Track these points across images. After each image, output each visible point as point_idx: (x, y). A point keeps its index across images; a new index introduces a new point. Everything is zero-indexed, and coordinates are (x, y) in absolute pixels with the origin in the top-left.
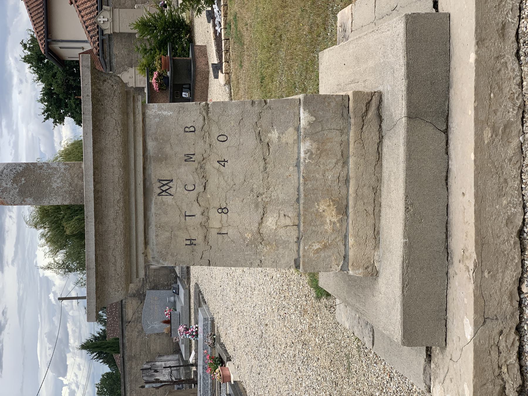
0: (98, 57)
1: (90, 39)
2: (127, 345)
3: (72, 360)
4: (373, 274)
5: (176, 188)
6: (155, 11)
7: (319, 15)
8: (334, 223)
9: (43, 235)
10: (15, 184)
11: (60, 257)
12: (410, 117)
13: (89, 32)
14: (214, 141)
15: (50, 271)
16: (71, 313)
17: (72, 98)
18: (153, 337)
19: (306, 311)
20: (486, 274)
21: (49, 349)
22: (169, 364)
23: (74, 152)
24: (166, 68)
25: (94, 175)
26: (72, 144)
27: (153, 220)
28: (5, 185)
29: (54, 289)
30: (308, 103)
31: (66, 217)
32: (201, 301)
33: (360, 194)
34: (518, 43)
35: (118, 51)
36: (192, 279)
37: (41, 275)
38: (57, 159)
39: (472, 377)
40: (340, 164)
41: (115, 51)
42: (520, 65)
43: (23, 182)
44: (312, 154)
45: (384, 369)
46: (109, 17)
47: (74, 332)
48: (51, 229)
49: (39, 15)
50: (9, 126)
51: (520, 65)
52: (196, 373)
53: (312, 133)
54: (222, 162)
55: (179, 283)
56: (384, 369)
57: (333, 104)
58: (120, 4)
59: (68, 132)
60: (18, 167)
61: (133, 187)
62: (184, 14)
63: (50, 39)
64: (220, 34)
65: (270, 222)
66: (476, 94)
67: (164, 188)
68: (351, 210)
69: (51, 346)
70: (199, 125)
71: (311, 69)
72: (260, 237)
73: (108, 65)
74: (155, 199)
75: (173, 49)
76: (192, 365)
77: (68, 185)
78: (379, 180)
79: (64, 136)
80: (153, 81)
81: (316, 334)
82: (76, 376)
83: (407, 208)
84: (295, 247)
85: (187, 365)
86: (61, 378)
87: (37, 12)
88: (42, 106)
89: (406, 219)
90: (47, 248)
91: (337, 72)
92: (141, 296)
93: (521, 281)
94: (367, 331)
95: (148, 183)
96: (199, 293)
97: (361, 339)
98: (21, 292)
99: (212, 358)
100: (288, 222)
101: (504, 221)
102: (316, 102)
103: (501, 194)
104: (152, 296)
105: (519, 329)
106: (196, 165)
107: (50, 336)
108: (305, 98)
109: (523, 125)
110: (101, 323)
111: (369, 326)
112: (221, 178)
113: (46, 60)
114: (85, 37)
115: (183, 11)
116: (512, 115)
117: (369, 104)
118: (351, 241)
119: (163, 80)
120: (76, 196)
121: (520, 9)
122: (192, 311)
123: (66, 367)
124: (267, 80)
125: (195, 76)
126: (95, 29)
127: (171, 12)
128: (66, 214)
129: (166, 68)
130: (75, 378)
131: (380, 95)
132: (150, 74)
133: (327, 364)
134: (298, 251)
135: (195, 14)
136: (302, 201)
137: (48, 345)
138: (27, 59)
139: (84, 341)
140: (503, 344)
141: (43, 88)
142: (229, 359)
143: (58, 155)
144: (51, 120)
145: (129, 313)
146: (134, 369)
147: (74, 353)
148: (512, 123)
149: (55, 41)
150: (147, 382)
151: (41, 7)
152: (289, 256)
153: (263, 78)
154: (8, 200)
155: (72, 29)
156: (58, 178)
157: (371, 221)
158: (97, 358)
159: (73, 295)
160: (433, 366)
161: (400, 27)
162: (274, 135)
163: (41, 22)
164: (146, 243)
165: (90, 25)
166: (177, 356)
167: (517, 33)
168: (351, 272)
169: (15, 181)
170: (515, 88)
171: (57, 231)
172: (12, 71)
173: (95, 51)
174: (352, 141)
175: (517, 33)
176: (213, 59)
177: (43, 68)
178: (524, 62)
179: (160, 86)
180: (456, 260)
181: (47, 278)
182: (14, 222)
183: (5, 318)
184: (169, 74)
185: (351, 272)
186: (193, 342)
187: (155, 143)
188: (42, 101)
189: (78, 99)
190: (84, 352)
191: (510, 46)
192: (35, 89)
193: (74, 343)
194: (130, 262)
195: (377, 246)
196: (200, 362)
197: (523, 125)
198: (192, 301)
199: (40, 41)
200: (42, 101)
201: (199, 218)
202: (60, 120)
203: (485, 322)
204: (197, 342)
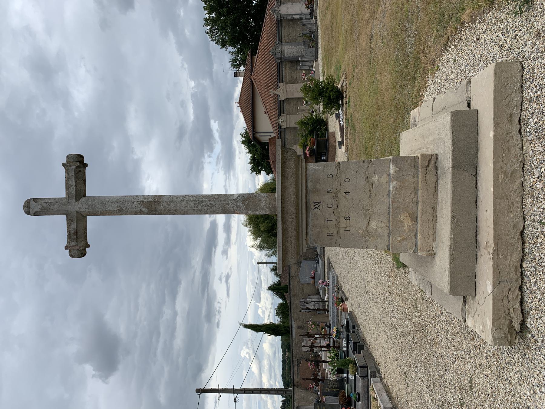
2: (292, 288)
4: (432, 255)
5: (322, 206)
6: (308, 115)
7: (399, 113)
8: (410, 226)
9: (250, 230)
11: (258, 242)
12: (454, 167)
14: (343, 182)
16: (263, 270)
18: (305, 285)
19: (391, 275)
20: (500, 256)
22: (314, 300)
23: (269, 188)
24: (313, 144)
27: (310, 223)
29: (255, 257)
30: (394, 161)
32: (331, 267)
33: (424, 210)
34: (520, 125)
35: (289, 136)
36: (326, 255)
39: (491, 314)
40: (413, 194)
42: (522, 137)
44: (397, 188)
45: (437, 308)
47: (264, 280)
48: (254, 227)
50: (234, 175)
51: (522, 137)
52: (328, 306)
53: (397, 177)
54: (347, 193)
55: (319, 257)
56: (437, 308)
57: (409, 161)
59: (263, 178)
61: (300, 205)
62: (323, 116)
64: (343, 125)
65: (373, 225)
66: (494, 154)
67: (316, 206)
68: (419, 219)
70: (335, 173)
71: (395, 143)
72: (367, 233)
74: (311, 211)
75: (317, 134)
76: (326, 301)
78: (436, 203)
79: (260, 180)
80: (307, 151)
81: (397, 288)
83: (452, 218)
84: (387, 239)
85: (324, 301)
86: (258, 304)
88: (250, 166)
89: (452, 224)
90: (252, 237)
91: (410, 143)
92: (299, 264)
93: (522, 261)
94: (428, 287)
95: (308, 204)
96: (330, 263)
97: (424, 291)
99: (337, 298)
100: (383, 225)
101: (512, 226)
102: (399, 160)
103: (509, 211)
104: (304, 263)
105: (521, 288)
106: (333, 194)
108: (393, 158)
109: (523, 172)
111: (429, 284)
112: (346, 201)
114: (271, 130)
115: (323, 114)
116: (517, 166)
117: (430, 160)
118: (419, 236)
119: (312, 151)
121: (521, 106)
122: (326, 273)
123: (260, 298)
124: (369, 149)
125: (329, 148)
127: (316, 115)
129: (313, 144)
131: (437, 156)
132: (305, 148)
133: (403, 304)
134: (389, 241)
135: (329, 115)
136: (391, 214)
137: (252, 286)
138: (243, 142)
140: (511, 296)
142: (347, 299)
144: (255, 172)
145: (293, 272)
146: (295, 302)
148: (517, 170)
150: (302, 309)
152: (384, 244)
153: (366, 148)
154: (240, 212)
155: (266, 127)
157: (431, 225)
159: (264, 261)
160: (467, 307)
161: (448, 118)
162: (376, 178)
164: (307, 235)
166: (318, 296)
167: (520, 119)
168: (419, 253)
169: (243, 202)
170: (518, 151)
173: (277, 137)
174: (420, 181)
175: (520, 119)
176: (339, 139)
178: (524, 136)
179: (310, 154)
180: (482, 248)
184: (315, 147)
185: (419, 253)
186: (327, 289)
187: (312, 183)
188: (250, 163)
190: (270, 291)
191: (515, 127)
192: (246, 157)
193: (265, 286)
194: (299, 244)
195: (434, 239)
196: (331, 300)
197: (523, 172)
198: (326, 267)
200: (250, 163)
201: (334, 222)
202: (259, 172)
203: (500, 283)
204: (329, 289)
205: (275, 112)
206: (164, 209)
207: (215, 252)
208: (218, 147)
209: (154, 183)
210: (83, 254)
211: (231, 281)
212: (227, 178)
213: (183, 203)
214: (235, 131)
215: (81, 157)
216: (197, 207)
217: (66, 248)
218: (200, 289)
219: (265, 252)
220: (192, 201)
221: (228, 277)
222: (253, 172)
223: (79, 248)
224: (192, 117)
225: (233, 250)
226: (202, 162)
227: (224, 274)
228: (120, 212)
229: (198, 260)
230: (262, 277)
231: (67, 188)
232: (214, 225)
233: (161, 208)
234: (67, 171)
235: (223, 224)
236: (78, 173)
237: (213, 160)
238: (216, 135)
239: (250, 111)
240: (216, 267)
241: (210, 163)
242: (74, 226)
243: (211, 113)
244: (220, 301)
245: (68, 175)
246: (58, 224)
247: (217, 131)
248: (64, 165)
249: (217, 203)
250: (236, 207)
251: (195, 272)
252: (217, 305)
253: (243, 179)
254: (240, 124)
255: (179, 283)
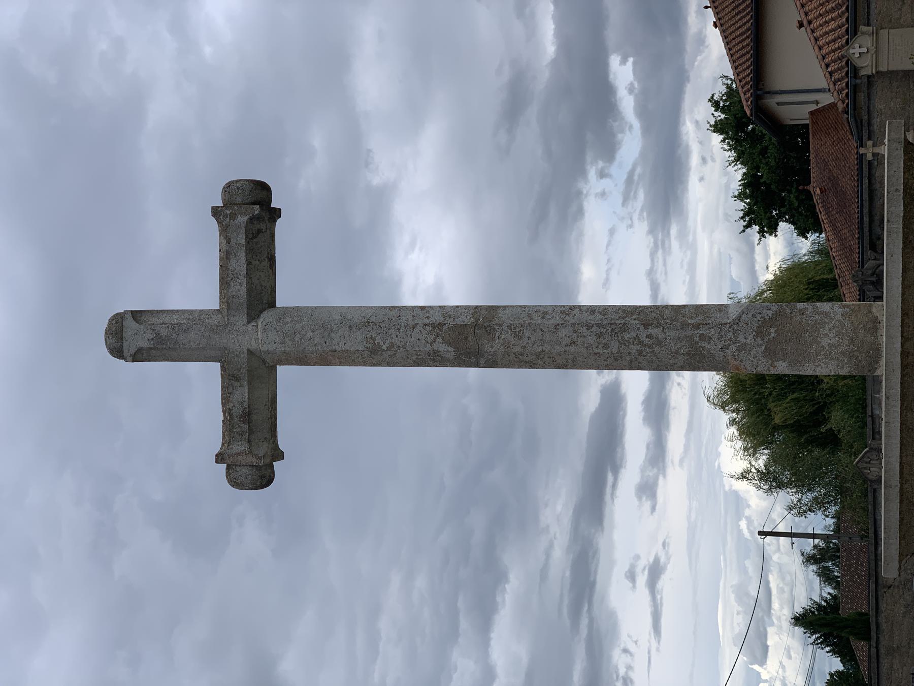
0: (846, 116)
1: (832, 86)
2: (884, 626)
3: (776, 638)
9: (733, 422)
10: (759, 339)
11: (761, 462)
13: (831, 74)
15: (745, 482)
16: (775, 558)
17: (794, 191)
21: (738, 613)
25: (902, 326)
26: (789, 269)
28: (743, 340)
29: (747, 512)
31: (774, 393)
37: (727, 488)
38: (762, 293)
41: (879, 104)
43: (773, 335)
46: (869, 45)
47: (781, 591)
48: (748, 413)
49: (744, 51)
50: (683, 235)
58: (890, 21)
59: (780, 249)
60: (764, 311)
63: (761, 90)
69: (741, 609)
73: (865, 128)
77: (847, 342)
82: (783, 667)
86: (756, 667)
87: (741, 46)
90: (739, 444)
98: (693, 516)
107: (740, 592)
110: (830, 584)
113: (750, 128)
120: (860, 361)
123: (766, 649)
126: (843, 68)
128: (775, 389)
130: (781, 671)
137: (737, 607)
138: (718, 128)
139: (799, 610)
141: (744, 174)
143: (764, 287)
147: (780, 627)
149: (769, 93)
151: (747, 37)
155: (802, 73)
156: (830, 330)
158: (821, 643)
159: (781, 529)
163: (747, 61)
165: (834, 61)
169: (759, 333)
171: (758, 417)
172: (690, 143)
173: (841, 106)
177: (744, 140)
181: (736, 494)
182: (685, 394)
183: (667, 553)
188: (741, 196)
189: (804, 190)
190: (799, 630)
193: (782, 611)
199: (745, 94)
200: (741, 196)
202: (769, 228)
205: (837, 22)
206: (502, 349)
207: (614, 486)
208: (631, 145)
209: (433, 261)
210: (264, 479)
211: (665, 583)
212: (659, 246)
213: (563, 333)
214: (689, 88)
215: (263, 188)
216: (606, 346)
217: (220, 458)
218: (566, 601)
219: (787, 496)
220: (589, 327)
221: (655, 571)
222: (748, 226)
223: (255, 461)
224: (550, 48)
225: (674, 485)
226: (579, 193)
227: (645, 561)
228: (376, 355)
229: (559, 508)
230: (774, 581)
231: (224, 282)
232: (613, 401)
233: (495, 347)
234: (224, 230)
235: (641, 398)
236: (254, 237)
237: (614, 185)
238: (627, 104)
239: (747, 21)
240: (617, 536)
241: (603, 194)
242: (242, 394)
243: (612, 35)
244: (632, 647)
245: (229, 242)
246: (196, 391)
247: (631, 90)
248: (216, 212)
249: (671, 333)
250: (733, 348)
251: (551, 545)
252: (619, 660)
253: (712, 250)
254: (711, 63)
255: (500, 577)
